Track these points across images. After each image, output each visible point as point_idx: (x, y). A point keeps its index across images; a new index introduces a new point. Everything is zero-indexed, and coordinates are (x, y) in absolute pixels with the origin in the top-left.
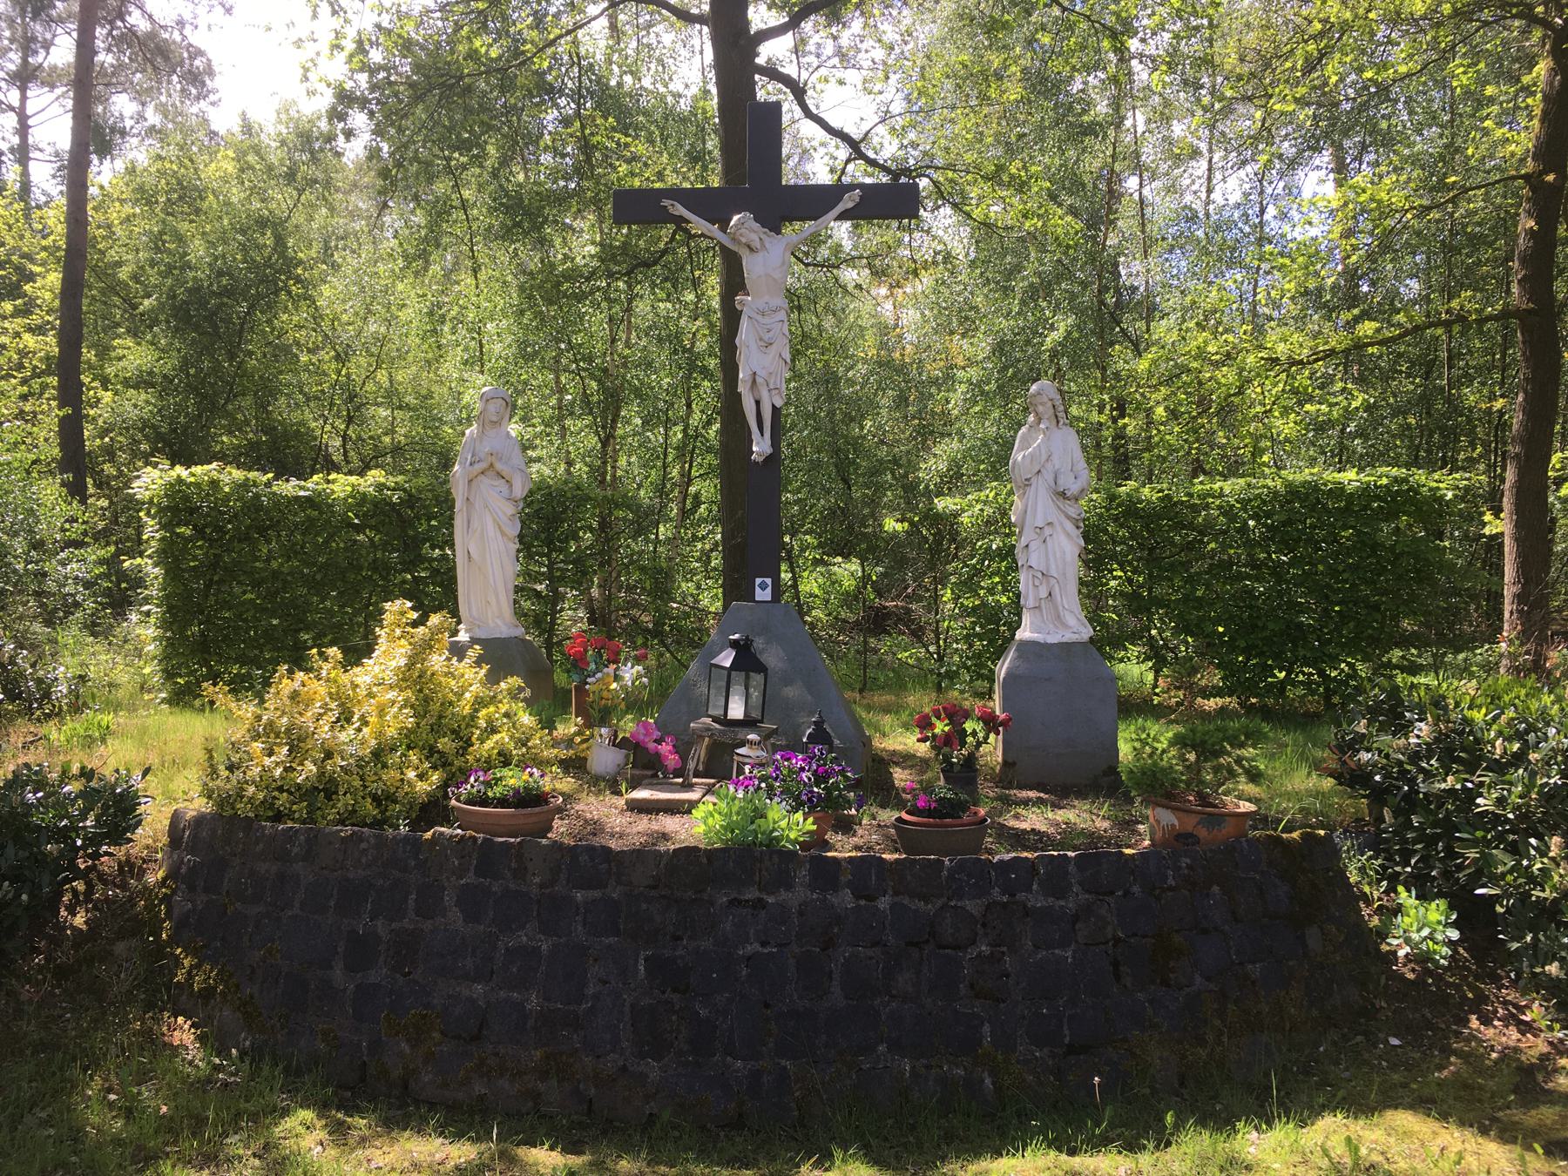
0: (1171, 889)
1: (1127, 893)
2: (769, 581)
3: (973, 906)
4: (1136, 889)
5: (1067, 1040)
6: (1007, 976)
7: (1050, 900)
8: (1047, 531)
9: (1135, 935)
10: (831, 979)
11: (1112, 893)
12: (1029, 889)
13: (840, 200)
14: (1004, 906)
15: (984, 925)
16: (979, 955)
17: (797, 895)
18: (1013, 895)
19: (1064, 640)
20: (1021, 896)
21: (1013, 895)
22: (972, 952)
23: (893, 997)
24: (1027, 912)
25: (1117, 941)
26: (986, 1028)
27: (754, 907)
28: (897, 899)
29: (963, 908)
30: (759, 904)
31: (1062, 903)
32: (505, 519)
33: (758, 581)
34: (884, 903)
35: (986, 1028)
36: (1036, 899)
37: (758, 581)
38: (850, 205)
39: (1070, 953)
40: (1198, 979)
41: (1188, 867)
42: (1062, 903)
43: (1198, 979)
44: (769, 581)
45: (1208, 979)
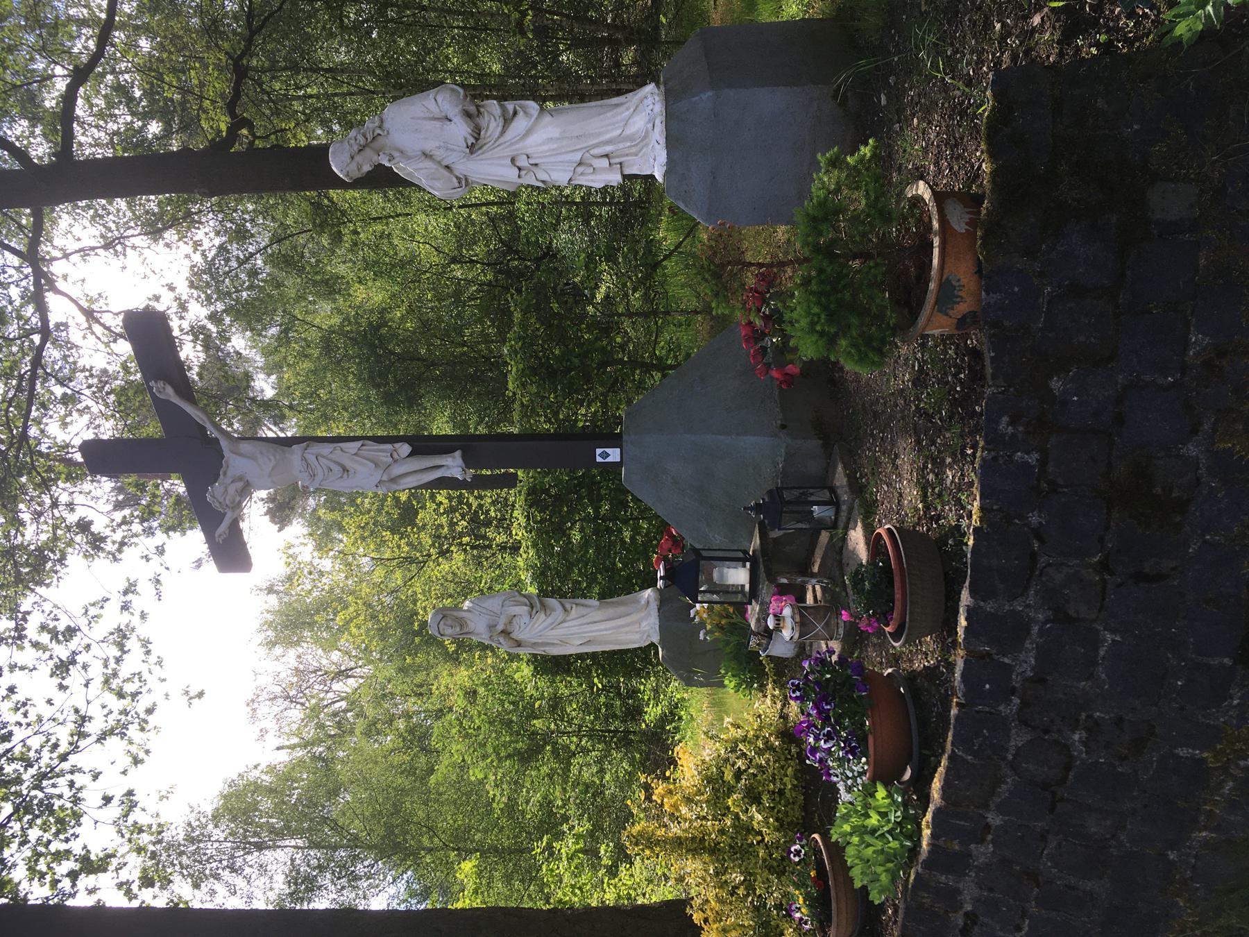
0: (1043, 462)
1: (1038, 534)
2: (599, 451)
3: (1018, 739)
4: (1034, 519)
5: (1227, 661)
6: (1121, 719)
7: (1028, 645)
8: (523, 162)
9: (1101, 539)
10: (1073, 888)
11: (1034, 556)
12: (1009, 669)
13: (168, 402)
14: (1025, 704)
15: (1046, 731)
16: (1085, 744)
17: (969, 892)
18: (1013, 691)
19: (663, 141)
20: (1016, 681)
21: (1013, 691)
22: (1079, 751)
23: (1113, 836)
24: (1039, 680)
25: (1104, 566)
26: (1182, 752)
27: (975, 923)
28: (992, 807)
29: (1018, 749)
30: (971, 917)
31: (1035, 629)
32: (549, 620)
33: (599, 459)
34: (994, 819)
35: (1182, 752)
36: (1025, 663)
37: (599, 459)
38: (170, 390)
39: (1109, 636)
40: (1192, 450)
41: (1012, 422)
42: (1035, 629)
43: (1192, 450)
44: (599, 451)
45: (1195, 431)
